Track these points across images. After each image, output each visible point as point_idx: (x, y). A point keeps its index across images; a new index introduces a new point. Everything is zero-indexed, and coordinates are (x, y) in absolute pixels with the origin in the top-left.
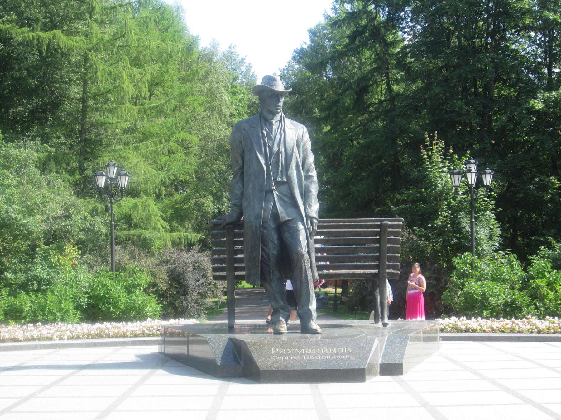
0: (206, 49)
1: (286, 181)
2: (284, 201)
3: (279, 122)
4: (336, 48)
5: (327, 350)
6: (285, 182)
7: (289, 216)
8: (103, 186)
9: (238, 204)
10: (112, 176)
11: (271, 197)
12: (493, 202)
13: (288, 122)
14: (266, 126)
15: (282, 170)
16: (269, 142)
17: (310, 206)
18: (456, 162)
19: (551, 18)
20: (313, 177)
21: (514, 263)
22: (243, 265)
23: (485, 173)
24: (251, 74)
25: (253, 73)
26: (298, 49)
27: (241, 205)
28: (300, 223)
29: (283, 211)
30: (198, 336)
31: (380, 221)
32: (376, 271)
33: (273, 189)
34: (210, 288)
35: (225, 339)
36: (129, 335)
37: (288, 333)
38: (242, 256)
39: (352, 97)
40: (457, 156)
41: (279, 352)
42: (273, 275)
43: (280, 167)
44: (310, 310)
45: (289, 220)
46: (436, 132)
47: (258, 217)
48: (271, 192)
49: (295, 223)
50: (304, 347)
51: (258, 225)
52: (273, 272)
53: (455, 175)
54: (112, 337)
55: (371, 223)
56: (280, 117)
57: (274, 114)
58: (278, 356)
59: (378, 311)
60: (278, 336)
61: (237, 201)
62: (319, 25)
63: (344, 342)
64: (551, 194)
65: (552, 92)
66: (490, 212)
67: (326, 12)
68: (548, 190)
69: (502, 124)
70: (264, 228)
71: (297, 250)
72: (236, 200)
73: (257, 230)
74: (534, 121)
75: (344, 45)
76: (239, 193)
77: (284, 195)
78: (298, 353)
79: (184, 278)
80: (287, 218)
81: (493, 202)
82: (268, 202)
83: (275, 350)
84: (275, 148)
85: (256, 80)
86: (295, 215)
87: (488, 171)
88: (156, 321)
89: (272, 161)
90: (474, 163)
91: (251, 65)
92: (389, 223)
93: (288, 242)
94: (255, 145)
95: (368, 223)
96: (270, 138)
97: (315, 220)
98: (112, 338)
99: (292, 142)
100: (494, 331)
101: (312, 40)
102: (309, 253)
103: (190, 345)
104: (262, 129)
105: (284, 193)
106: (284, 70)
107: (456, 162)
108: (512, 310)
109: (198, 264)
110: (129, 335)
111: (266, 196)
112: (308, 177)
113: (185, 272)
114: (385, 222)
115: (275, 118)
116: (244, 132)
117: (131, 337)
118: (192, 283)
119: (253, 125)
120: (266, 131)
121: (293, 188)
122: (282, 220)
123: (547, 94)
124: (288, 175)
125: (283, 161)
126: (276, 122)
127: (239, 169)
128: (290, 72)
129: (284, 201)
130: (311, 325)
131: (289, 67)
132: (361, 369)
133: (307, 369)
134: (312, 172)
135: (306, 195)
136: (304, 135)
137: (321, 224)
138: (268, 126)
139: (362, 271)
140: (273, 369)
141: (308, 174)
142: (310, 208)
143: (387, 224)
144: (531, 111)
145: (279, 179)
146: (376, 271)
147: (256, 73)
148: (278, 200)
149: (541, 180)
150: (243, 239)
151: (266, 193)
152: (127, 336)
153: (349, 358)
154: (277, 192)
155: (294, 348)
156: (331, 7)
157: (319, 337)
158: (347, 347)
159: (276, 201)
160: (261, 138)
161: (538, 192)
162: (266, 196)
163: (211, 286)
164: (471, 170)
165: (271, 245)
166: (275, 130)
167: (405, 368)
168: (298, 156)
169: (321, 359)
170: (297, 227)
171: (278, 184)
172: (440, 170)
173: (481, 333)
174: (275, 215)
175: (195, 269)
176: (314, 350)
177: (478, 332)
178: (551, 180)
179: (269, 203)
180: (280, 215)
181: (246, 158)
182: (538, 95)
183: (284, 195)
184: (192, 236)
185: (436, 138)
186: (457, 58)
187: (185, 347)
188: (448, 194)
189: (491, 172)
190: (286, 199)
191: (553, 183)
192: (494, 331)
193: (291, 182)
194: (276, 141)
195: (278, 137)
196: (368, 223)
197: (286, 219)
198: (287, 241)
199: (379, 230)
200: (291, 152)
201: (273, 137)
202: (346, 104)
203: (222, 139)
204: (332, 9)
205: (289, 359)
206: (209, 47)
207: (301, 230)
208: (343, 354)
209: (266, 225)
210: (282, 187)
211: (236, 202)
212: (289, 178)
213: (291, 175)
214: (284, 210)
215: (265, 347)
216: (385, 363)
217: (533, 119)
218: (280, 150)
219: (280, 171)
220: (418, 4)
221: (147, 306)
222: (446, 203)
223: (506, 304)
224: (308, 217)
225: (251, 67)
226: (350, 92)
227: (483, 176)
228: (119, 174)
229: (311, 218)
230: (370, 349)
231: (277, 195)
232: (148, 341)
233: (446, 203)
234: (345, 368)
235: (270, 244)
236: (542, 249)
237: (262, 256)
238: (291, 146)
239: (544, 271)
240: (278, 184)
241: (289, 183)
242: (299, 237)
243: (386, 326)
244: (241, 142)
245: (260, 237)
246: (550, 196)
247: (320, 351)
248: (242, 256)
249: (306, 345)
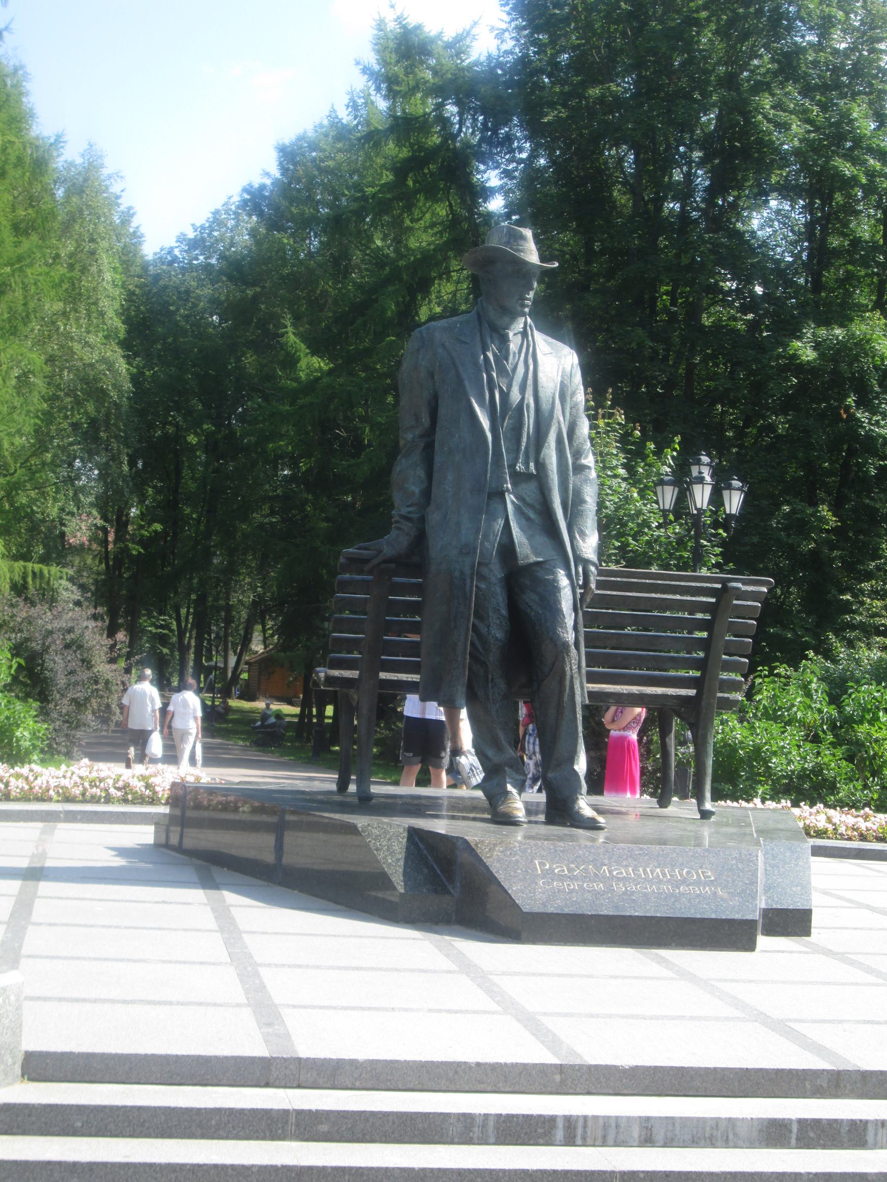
0: (71, 164)
1: (534, 472)
2: (528, 519)
3: (519, 336)
4: (362, 191)
5: (658, 870)
6: (532, 474)
7: (537, 554)
9: (415, 516)
11: (500, 507)
12: (718, 550)
13: (542, 342)
14: (492, 342)
15: (527, 448)
16: (501, 379)
17: (583, 534)
18: (652, 458)
19: (847, 172)
20: (589, 468)
21: (814, 686)
22: (356, 655)
23: (729, 487)
24: (131, 230)
25: (137, 228)
26: (252, 187)
27: (422, 520)
28: (562, 572)
29: (525, 541)
30: (310, 814)
31: (724, 582)
32: (692, 692)
33: (508, 490)
34: (97, 690)
35: (401, 830)
36: (55, 797)
37: (530, 822)
38: (416, 638)
39: (401, 299)
40: (652, 446)
41: (552, 870)
42: (493, 687)
43: (524, 439)
44: (576, 774)
45: (537, 564)
46: (610, 390)
47: (468, 550)
48: (500, 495)
49: (551, 570)
50: (606, 862)
51: (468, 572)
52: (493, 679)
53: (665, 487)
54: (16, 800)
55: (698, 585)
56: (522, 326)
57: (513, 316)
58: (553, 880)
59: (670, 780)
60: (506, 829)
61: (410, 509)
62: (301, 138)
63: (691, 854)
64: (815, 541)
65: (833, 329)
66: (708, 569)
67: (334, 111)
68: (809, 534)
69: (726, 386)
70: (482, 577)
71: (555, 633)
72: (408, 506)
73: (465, 580)
74: (792, 386)
75: (383, 186)
76: (417, 491)
79: (42, 665)
80: (533, 559)
81: (718, 550)
82: (492, 518)
83: (542, 864)
84: (515, 396)
85: (140, 243)
86: (550, 553)
87: (736, 483)
89: (505, 424)
90: (707, 465)
91: (132, 212)
92: (745, 588)
93: (533, 613)
94: (467, 383)
95: (693, 584)
96: (502, 371)
98: (13, 800)
100: (863, 838)
101: (284, 170)
103: (286, 833)
104: (485, 349)
105: (527, 499)
106: (203, 227)
107: (652, 458)
108: (816, 787)
109: (72, 636)
110: (55, 797)
111: (488, 505)
112: (580, 469)
113: (46, 649)
114: (735, 584)
115: (512, 327)
116: (440, 350)
117: (58, 801)
118: (62, 681)
119: (463, 339)
120: (495, 355)
121: (550, 490)
122: (521, 562)
123: (823, 332)
124: (541, 460)
125: (531, 427)
126: (515, 334)
127: (421, 436)
129: (528, 519)
130: (580, 808)
131: (213, 222)
132: (747, 920)
133: (628, 914)
134: (586, 457)
137: (603, 578)
138: (497, 342)
139: (659, 690)
140: (550, 909)
141: (579, 462)
142: (584, 540)
143: (738, 589)
144: (794, 365)
145: (520, 467)
146: (692, 692)
147: (142, 230)
148: (515, 514)
149: (793, 511)
151: (490, 496)
152: (50, 799)
153: (715, 893)
154: (512, 496)
155: (584, 862)
156: (346, 102)
157: (601, 837)
158: (701, 867)
159: (511, 517)
160: (483, 369)
161: (789, 535)
162: (488, 505)
163: (100, 687)
164: (703, 479)
166: (514, 353)
167: (816, 920)
168: (561, 419)
170: (555, 580)
171: (518, 478)
172: (609, 473)
173: (836, 838)
174: (508, 549)
175: (67, 646)
176: (630, 869)
177: (829, 838)
178: (820, 512)
179: (495, 520)
180: (518, 549)
181: (442, 411)
182: (804, 331)
184: (53, 573)
185: (609, 403)
186: (639, 237)
187: (269, 840)
188: (624, 525)
189: (742, 487)
190: (532, 515)
191: (823, 520)
192: (863, 838)
193: (546, 476)
194: (516, 378)
195: (521, 370)
196: (693, 584)
197: (531, 561)
198: (529, 610)
199: (713, 600)
200: (549, 407)
201: (509, 368)
202: (389, 313)
203: (92, 365)
204: (348, 106)
205: (581, 887)
206: (79, 161)
207: (565, 587)
208: (698, 883)
209: (485, 571)
210: (524, 486)
211: (409, 512)
212: (541, 466)
213: (547, 461)
214: (528, 539)
215: (517, 857)
216: (774, 907)
217: (791, 381)
218: (526, 402)
219: (523, 448)
220: (560, 112)
221: (18, 726)
222: (617, 544)
223: (803, 775)
224: (579, 559)
225: (132, 215)
226: (397, 287)
227: (726, 493)
229: (586, 562)
230: (755, 873)
231: (513, 502)
232: (104, 813)
233: (617, 544)
234: (713, 916)
236: (810, 656)
237: (472, 644)
239: (878, 708)
240: (518, 478)
241: (540, 478)
242: (560, 604)
243: (709, 818)
244: (432, 375)
245: (471, 596)
246: (813, 545)
248: (416, 638)
249: (610, 858)
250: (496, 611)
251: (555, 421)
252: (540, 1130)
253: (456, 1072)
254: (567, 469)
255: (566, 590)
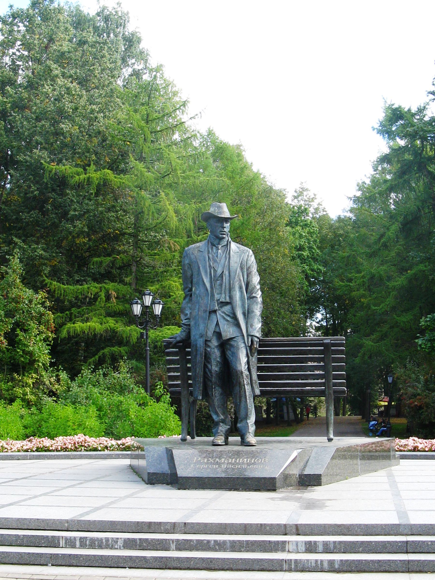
8: (159, 314)
10: (147, 305)
17: (252, 326)
61: (186, 321)
72: (185, 320)
77: (227, 315)
78: (217, 462)
88: (176, 436)
97: (256, 339)
99: (236, 265)
102: (249, 370)
105: (226, 312)
111: (209, 316)
126: (222, 246)
128: (431, 207)
135: (247, 314)
136: (249, 259)
150: (190, 357)
151: (210, 313)
162: (209, 316)
165: (214, 363)
166: (221, 254)
168: (242, 279)
169: (238, 468)
183: (227, 315)
195: (223, 261)
211: (186, 322)
228: (153, 303)
235: (212, 361)
238: (235, 268)
247: (239, 460)
250: (215, 359)
251: (237, 278)
252: (43, 541)
253: (30, 522)
254: (245, 298)
255: (243, 349)
